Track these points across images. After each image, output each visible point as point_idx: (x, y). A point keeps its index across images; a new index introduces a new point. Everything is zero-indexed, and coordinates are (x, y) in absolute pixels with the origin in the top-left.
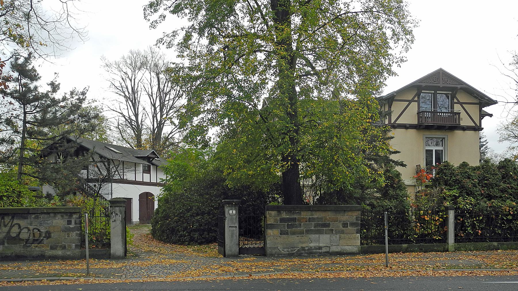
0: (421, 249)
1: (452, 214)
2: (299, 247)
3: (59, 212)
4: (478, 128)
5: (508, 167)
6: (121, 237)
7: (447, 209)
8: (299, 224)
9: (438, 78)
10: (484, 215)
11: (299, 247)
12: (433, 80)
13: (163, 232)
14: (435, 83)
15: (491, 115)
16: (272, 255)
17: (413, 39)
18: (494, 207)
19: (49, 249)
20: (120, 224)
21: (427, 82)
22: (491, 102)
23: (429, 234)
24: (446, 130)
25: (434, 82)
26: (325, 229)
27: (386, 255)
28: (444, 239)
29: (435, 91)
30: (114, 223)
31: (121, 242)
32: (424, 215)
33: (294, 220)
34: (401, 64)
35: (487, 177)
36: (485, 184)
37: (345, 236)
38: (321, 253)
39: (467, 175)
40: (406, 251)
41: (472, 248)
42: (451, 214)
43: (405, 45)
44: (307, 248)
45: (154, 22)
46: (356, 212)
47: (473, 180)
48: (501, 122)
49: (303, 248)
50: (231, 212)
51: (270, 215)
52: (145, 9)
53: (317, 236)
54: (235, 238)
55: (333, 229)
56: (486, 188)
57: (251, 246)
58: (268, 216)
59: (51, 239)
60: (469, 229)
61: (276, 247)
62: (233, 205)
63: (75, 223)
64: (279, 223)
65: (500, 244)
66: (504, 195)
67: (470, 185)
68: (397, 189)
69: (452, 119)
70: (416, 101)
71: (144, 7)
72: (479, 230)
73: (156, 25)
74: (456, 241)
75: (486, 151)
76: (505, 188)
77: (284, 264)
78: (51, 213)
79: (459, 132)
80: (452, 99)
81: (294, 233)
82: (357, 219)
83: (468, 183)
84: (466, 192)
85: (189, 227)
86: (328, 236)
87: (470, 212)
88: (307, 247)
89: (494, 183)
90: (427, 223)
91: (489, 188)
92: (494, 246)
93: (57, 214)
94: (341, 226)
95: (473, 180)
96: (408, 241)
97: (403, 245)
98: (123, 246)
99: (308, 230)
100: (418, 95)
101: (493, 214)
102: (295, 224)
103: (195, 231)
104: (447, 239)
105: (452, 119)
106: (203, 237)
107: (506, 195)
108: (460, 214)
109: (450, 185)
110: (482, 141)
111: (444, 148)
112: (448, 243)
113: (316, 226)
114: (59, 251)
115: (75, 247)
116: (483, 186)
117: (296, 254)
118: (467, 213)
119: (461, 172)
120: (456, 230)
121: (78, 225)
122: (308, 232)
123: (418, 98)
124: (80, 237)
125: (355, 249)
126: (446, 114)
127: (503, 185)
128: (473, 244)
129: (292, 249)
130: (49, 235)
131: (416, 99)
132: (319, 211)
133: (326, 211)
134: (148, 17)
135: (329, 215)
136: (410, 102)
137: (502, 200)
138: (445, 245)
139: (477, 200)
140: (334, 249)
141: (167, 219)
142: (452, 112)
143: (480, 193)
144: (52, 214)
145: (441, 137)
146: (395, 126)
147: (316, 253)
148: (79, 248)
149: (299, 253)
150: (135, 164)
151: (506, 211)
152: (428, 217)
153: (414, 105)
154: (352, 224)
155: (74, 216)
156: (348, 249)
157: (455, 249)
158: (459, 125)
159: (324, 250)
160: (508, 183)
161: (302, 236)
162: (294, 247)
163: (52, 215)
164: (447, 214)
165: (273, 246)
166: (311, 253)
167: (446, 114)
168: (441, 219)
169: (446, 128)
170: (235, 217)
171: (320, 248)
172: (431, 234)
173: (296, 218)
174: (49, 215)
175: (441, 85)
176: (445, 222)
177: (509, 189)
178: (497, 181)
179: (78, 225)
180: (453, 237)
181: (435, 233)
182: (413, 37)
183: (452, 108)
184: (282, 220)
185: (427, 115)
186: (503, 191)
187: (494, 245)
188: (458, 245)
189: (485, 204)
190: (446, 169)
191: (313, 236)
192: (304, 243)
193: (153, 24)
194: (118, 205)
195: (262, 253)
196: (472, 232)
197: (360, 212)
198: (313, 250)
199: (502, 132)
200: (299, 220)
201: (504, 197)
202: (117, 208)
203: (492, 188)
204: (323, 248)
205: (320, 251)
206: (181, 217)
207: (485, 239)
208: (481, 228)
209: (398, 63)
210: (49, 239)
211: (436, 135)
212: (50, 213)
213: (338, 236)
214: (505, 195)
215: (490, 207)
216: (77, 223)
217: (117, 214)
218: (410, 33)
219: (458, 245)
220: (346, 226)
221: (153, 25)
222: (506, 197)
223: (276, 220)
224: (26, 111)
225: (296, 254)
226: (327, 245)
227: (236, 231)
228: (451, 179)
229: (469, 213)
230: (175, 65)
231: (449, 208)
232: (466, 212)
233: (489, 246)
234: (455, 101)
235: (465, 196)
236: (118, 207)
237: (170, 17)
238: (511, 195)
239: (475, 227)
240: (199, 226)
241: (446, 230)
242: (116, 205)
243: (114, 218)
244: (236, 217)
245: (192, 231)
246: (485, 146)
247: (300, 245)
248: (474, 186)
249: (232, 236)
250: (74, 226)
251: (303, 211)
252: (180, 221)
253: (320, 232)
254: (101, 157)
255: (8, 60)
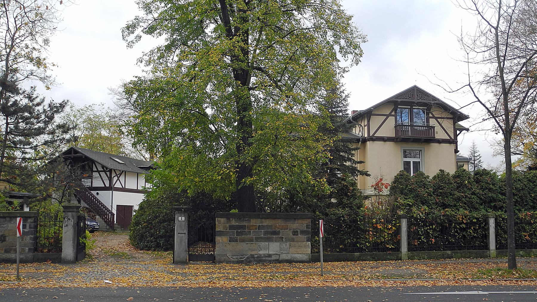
0: (374, 258)
1: (405, 223)
2: (248, 255)
3: (14, 216)
4: (453, 141)
5: (463, 177)
6: (72, 241)
7: (400, 217)
8: (249, 231)
9: (413, 95)
10: (437, 224)
11: (248, 255)
12: (408, 96)
13: (135, 238)
14: (410, 98)
15: (467, 130)
16: (220, 262)
17: (362, 53)
18: (448, 215)
19: (3, 252)
20: (72, 229)
21: (403, 98)
22: (464, 117)
23: (382, 242)
24: (422, 142)
25: (409, 97)
26: (274, 236)
27: (322, 264)
28: (398, 249)
29: (412, 106)
30: (66, 227)
31: (72, 246)
32: (376, 223)
33: (243, 227)
34: (344, 75)
35: (441, 186)
36: (441, 193)
37: (295, 244)
38: (271, 261)
39: (422, 184)
40: (359, 259)
41: (426, 257)
42: (404, 224)
43: (355, 58)
44: (257, 256)
45: (130, 43)
46: (306, 219)
47: (428, 189)
48: (494, 138)
49: (252, 256)
50: (180, 218)
51: (219, 222)
52: (123, 31)
53: (267, 243)
54: (183, 244)
55: (283, 236)
56: (441, 197)
57: (209, 253)
58: (217, 223)
59: (5, 242)
60: (422, 237)
61: (225, 255)
62: (183, 212)
63: (30, 227)
64: (228, 230)
65: (454, 252)
66: (458, 204)
67: (426, 195)
68: (351, 197)
69: (427, 132)
70: (393, 116)
71: (122, 29)
72: (432, 238)
73: (133, 45)
74: (409, 250)
75: (480, 164)
76: (459, 197)
77: (230, 270)
78: (8, 217)
79: (435, 145)
80: (428, 114)
81: (243, 241)
82: (307, 227)
83: (423, 192)
84: (421, 201)
85: (156, 233)
86: (278, 244)
87: (424, 221)
88: (257, 254)
89: (449, 192)
90: (380, 231)
91: (444, 198)
92: (448, 254)
93: (12, 218)
94: (291, 234)
95: (428, 189)
96: (361, 250)
97: (355, 254)
98: (74, 250)
99: (258, 237)
100: (395, 110)
101: (446, 223)
102: (245, 231)
103: (161, 237)
104: (400, 247)
105: (427, 132)
106: (169, 244)
107: (461, 204)
108: (413, 222)
109: (406, 195)
110: (475, 155)
111: (421, 160)
112: (401, 252)
113: (266, 234)
114: (12, 254)
115: (28, 251)
116: (437, 195)
117: (245, 262)
118: (420, 221)
119: (416, 181)
120: (410, 239)
121: (32, 230)
122: (258, 239)
123: (396, 112)
124: (33, 241)
125: (306, 258)
126: (421, 128)
127: (457, 194)
128: (426, 253)
129: (241, 256)
130: (4, 238)
131: (393, 113)
132: (268, 218)
133: (276, 218)
134: (127, 38)
135: (279, 223)
136: (388, 116)
137: (457, 209)
138: (399, 254)
139: (432, 209)
140: (284, 257)
141: (138, 226)
142: (428, 126)
143: (435, 201)
144: (8, 218)
145: (418, 149)
146: (373, 139)
147: (265, 261)
148: (32, 252)
149: (248, 260)
150: (138, 174)
151: (459, 220)
152: (380, 225)
153: (391, 120)
154: (303, 232)
155: (29, 220)
156: (298, 258)
157: (408, 257)
158: (433, 138)
159: (274, 258)
160: (462, 192)
161: (252, 244)
162: (243, 254)
163: (8, 219)
164: (400, 222)
165: (222, 253)
166: (260, 261)
167: (421, 128)
168: (394, 228)
169: (423, 141)
170: (184, 223)
171: (270, 256)
172: (383, 242)
173: (245, 225)
174: (5, 219)
175: (416, 101)
176: (398, 231)
177: (463, 197)
178: (451, 190)
179: (32, 230)
180: (406, 246)
181: (389, 242)
182: (361, 51)
183: (428, 121)
184: (231, 227)
185: (405, 129)
186: (459, 199)
187: (447, 254)
188: (411, 253)
189: (439, 212)
190: (402, 178)
191: (263, 243)
192: (254, 250)
193: (130, 44)
194: (71, 210)
195: (212, 259)
196: (425, 241)
197: (310, 220)
198: (262, 257)
199: (495, 147)
200: (249, 227)
201: (459, 206)
202: (70, 214)
203: (447, 197)
204: (272, 256)
205: (270, 259)
206: (149, 223)
207: (439, 247)
208: (435, 236)
209: (341, 74)
210: (3, 243)
211: (407, 147)
212: (6, 217)
213: (288, 244)
214: (460, 204)
215: (443, 216)
216: (31, 228)
217: (69, 219)
218: (356, 47)
219: (411, 253)
220: (296, 233)
221: (130, 45)
222: (460, 206)
223: (225, 227)
224: (8, 122)
225: (245, 262)
226: (277, 253)
227: (185, 238)
228: (406, 188)
229: (422, 222)
230: (137, 78)
231: (402, 216)
232: (419, 220)
233: (443, 255)
234: (430, 115)
235: (420, 205)
236: (70, 212)
237: (146, 38)
238: (465, 203)
239: (429, 236)
240: (165, 233)
241: (400, 238)
242: (69, 210)
243: (66, 223)
244: (185, 223)
245: (158, 237)
246: (479, 160)
247: (250, 253)
248: (429, 195)
249: (181, 242)
250: (29, 230)
251: (252, 218)
252: (148, 227)
253: (269, 240)
254: (103, 167)
255: (24, 79)
